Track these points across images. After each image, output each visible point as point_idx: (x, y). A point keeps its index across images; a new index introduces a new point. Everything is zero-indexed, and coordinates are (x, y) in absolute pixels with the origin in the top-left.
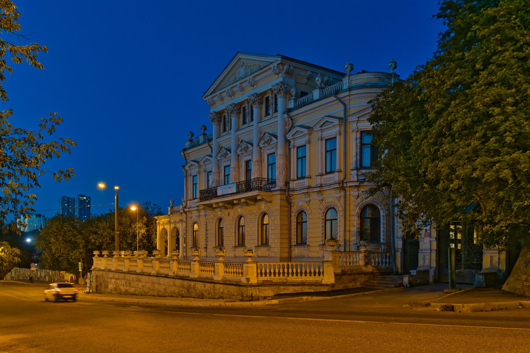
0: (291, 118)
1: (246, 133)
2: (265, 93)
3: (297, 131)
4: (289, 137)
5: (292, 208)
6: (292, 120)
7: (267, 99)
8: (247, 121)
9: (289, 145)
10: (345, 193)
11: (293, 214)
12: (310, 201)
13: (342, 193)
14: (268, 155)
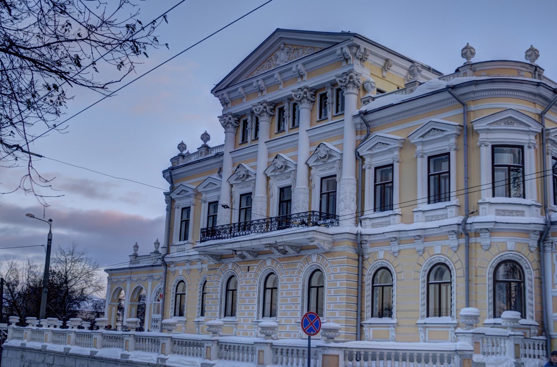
0: (367, 124)
1: (322, 136)
2: (323, 87)
3: (377, 143)
4: (363, 152)
5: (366, 263)
6: (368, 126)
7: (245, 123)
8: (249, 139)
9: (363, 164)
10: (468, 240)
11: (366, 272)
12: (399, 251)
13: (462, 241)
14: (322, 179)
